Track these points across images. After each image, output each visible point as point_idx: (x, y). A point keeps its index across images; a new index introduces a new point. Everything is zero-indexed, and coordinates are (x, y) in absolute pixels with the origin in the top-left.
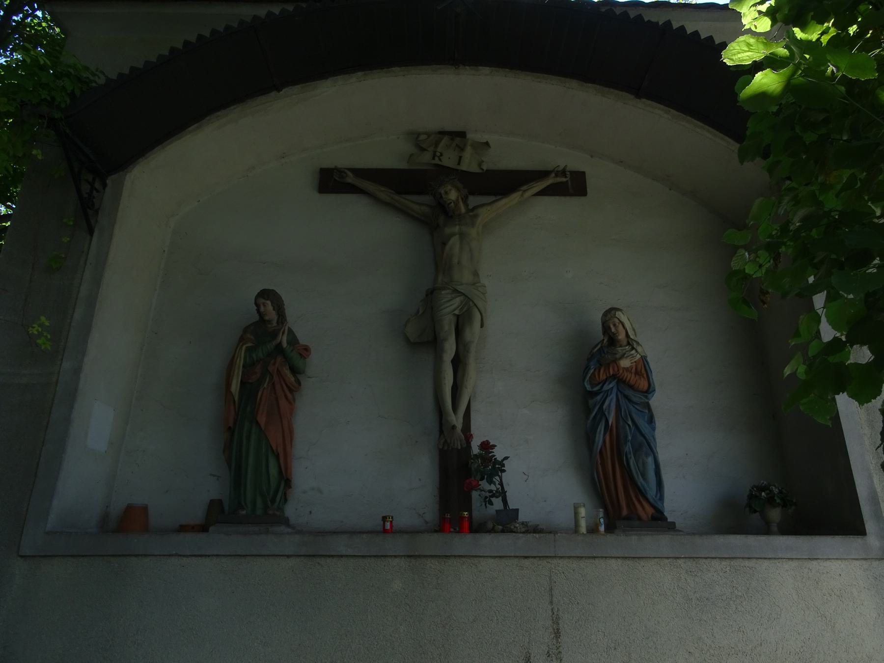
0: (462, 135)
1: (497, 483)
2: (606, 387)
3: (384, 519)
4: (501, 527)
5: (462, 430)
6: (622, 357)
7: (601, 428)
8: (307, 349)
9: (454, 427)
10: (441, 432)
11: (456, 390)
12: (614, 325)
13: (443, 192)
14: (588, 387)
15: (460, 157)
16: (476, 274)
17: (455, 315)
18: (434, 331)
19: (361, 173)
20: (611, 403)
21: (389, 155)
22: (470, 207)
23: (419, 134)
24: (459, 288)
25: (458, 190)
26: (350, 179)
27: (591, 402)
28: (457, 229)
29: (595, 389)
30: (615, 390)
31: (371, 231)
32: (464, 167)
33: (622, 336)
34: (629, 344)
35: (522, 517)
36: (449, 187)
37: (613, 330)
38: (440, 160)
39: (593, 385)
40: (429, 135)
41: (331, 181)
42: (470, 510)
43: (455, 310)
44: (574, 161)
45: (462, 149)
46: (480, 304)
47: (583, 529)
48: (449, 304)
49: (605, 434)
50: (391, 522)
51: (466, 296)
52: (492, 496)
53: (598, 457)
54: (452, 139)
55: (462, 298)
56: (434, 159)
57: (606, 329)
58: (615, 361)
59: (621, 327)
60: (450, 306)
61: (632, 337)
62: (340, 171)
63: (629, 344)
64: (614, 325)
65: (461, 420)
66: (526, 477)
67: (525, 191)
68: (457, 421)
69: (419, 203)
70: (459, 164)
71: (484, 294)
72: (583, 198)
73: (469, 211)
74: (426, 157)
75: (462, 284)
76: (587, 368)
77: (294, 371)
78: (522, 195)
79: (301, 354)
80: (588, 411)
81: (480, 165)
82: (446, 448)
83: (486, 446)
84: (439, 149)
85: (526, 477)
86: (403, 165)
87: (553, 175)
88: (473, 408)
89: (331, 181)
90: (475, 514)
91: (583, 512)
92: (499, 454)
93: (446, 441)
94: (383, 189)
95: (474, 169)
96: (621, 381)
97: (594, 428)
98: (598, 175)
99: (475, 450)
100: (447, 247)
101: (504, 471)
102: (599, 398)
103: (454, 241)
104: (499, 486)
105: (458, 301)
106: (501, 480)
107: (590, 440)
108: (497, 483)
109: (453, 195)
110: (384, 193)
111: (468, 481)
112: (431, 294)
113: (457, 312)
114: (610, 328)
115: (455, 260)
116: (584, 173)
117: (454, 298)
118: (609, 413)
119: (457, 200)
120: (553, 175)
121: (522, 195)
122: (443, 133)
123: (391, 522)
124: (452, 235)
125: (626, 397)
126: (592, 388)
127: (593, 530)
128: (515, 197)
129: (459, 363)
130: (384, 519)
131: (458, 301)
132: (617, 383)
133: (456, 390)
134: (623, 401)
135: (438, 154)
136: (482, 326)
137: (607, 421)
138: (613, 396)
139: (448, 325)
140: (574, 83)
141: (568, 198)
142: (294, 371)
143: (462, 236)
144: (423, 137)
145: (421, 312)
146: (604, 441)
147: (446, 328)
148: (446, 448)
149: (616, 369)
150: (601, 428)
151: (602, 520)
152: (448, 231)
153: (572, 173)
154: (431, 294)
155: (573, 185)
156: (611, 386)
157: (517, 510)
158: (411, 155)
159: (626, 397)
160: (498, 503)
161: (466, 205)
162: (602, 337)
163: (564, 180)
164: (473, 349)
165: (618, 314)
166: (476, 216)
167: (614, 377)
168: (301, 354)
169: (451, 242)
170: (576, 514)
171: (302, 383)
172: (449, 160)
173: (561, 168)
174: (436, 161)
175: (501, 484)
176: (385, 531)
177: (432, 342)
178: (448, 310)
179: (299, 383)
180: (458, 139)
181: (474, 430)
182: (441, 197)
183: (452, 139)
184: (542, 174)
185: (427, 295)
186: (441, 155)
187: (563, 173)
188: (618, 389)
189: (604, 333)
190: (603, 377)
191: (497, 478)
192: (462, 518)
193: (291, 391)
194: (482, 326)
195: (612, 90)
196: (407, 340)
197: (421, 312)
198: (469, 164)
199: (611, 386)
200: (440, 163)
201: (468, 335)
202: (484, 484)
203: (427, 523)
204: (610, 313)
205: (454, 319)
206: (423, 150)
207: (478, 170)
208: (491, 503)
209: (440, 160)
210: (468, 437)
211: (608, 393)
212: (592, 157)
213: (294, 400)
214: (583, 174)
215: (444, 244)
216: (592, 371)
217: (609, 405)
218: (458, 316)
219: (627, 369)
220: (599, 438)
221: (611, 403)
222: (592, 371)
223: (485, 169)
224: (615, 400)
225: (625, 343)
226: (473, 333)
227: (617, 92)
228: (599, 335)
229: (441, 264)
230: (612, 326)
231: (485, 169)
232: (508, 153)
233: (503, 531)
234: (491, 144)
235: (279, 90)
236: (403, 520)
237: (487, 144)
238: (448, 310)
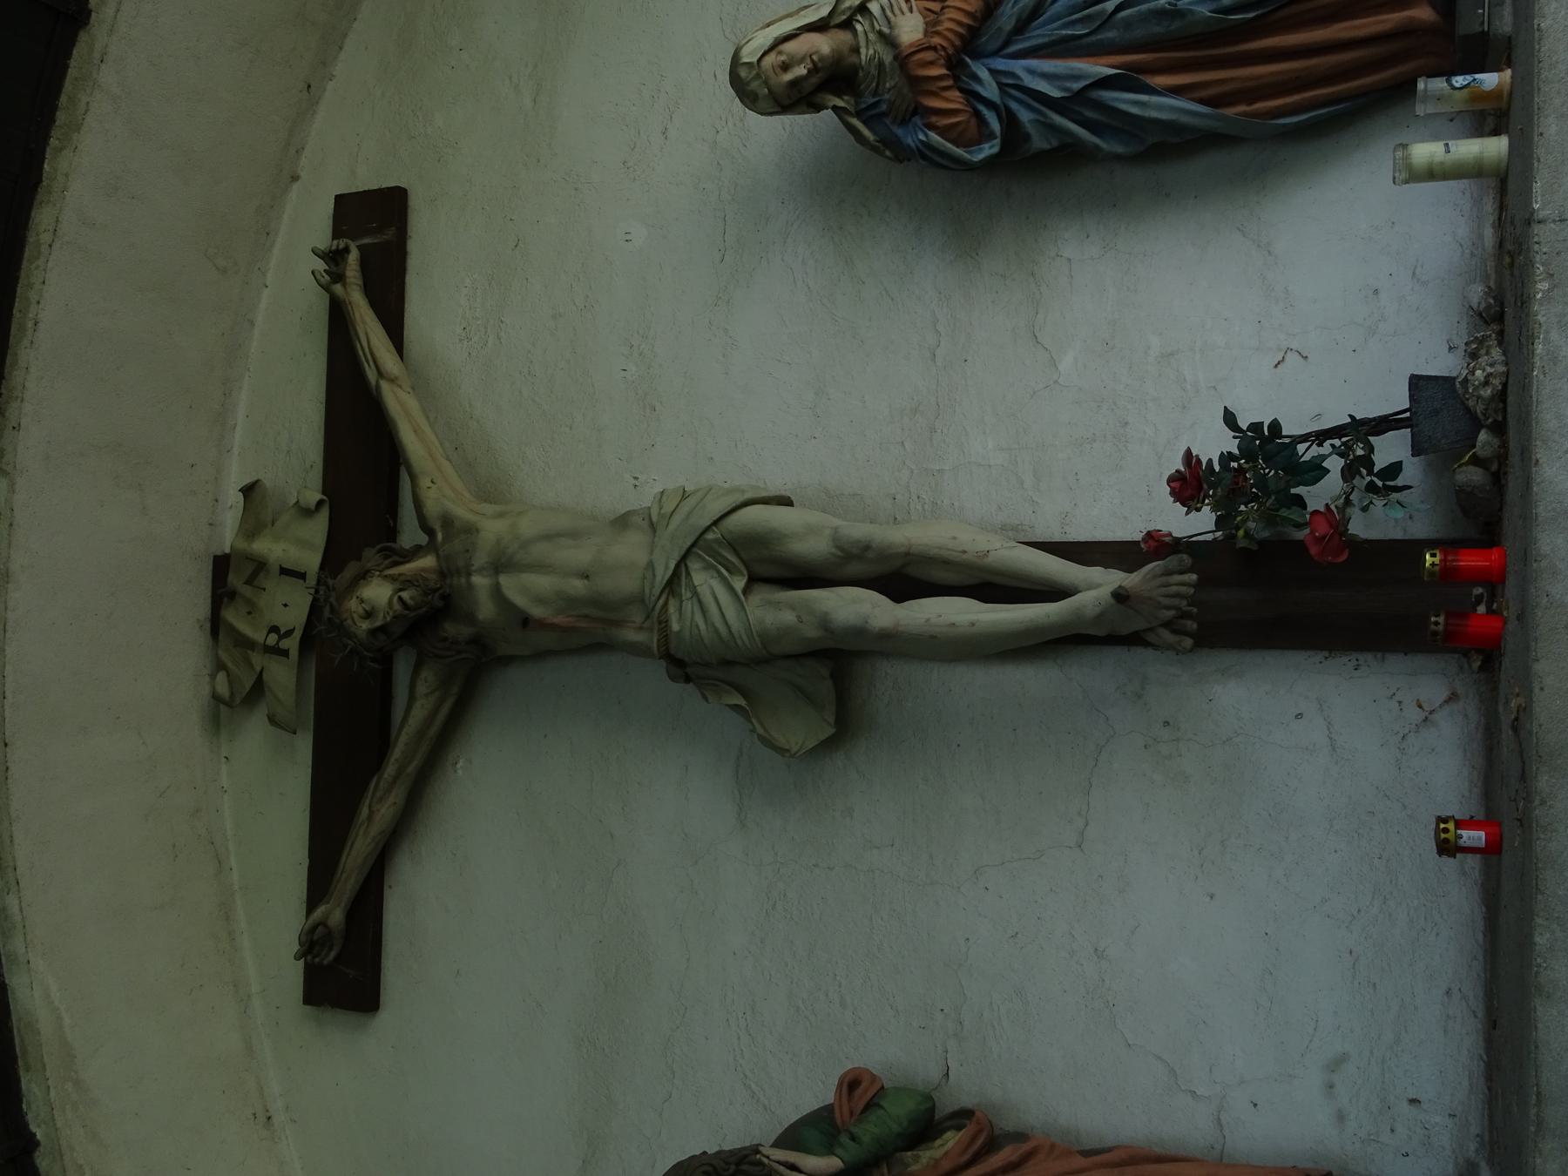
0: (221, 565)
1: (1315, 450)
2: (990, 90)
3: (1447, 848)
4: (1483, 436)
5: (1130, 571)
6: (889, 40)
7: (1124, 101)
8: (852, 1083)
9: (1120, 596)
10: (1135, 640)
11: (993, 586)
12: (785, 67)
13: (365, 625)
14: (988, 150)
15: (285, 572)
16: (622, 522)
17: (746, 591)
18: (804, 657)
19: (319, 885)
20: (1044, 75)
21: (266, 791)
22: (423, 539)
23: (216, 697)
24: (663, 574)
25: (364, 576)
26: (334, 913)
27: (1039, 142)
28: (480, 581)
29: (995, 125)
30: (1000, 64)
31: (524, 843)
32: (311, 561)
33: (823, 44)
34: (847, 25)
35: (1442, 363)
36: (353, 604)
37: (801, 71)
38: (289, 633)
39: (984, 135)
40: (220, 666)
41: (344, 972)
42: (1414, 548)
43: (731, 589)
44: (308, 223)
45: (260, 566)
46: (716, 507)
47: (1495, 147)
48: (713, 609)
49: (1152, 91)
50: (1459, 824)
51: (683, 559)
52: (1367, 461)
53: (1230, 111)
54: (232, 595)
55: (694, 565)
56: (285, 653)
57: (795, 98)
58: (903, 60)
59: (789, 47)
60: (720, 605)
61: (825, 12)
62: (311, 944)
63: (847, 25)
64: (785, 67)
65: (1095, 573)
66: (1292, 358)
67: (380, 374)
68: (1097, 586)
69: (415, 701)
70: (302, 576)
71: (685, 495)
72: (416, 202)
73: (432, 547)
74: (281, 676)
75: (650, 565)
76: (928, 155)
77: (925, 1128)
78: (393, 380)
79: (869, 1106)
80: (1069, 156)
81: (307, 512)
82: (1192, 625)
83: (1190, 484)
84: (259, 636)
85: (1292, 358)
86: (304, 746)
87: (338, 288)
88: (1057, 537)
89: (344, 972)
90: (1420, 529)
91: (1426, 151)
92: (1214, 444)
93: (1167, 625)
94: (365, 812)
95: (317, 530)
96: (970, 44)
97: (1130, 126)
98: (345, 159)
99: (1200, 523)
100: (537, 612)
101: (1275, 426)
102: (1025, 116)
103: (521, 589)
104: (1326, 448)
105: (702, 579)
106: (1304, 438)
107: (1164, 148)
108: (1315, 450)
109: (378, 592)
110: (378, 812)
111: (1313, 550)
112: (688, 666)
113: (739, 583)
114: (794, 83)
115: (577, 586)
116: (339, 199)
117: (695, 594)
118: (1076, 77)
119: (393, 579)
120: (338, 288)
121: (393, 380)
122: (216, 625)
123: (1459, 824)
124: (497, 592)
125: (1022, 27)
126: (992, 136)
127: (1489, 116)
128: (399, 402)
129: (904, 578)
130: (1447, 848)
131: (702, 579)
132: (977, 56)
133: (993, 586)
134: (1039, 35)
135: (272, 639)
136: (786, 502)
137: (1105, 83)
138: (1018, 66)
139: (779, 612)
140: (42, 217)
141: (413, 246)
142: (925, 1128)
143: (501, 564)
144: (223, 688)
145: (742, 702)
146: (1176, 91)
147: (788, 617)
148: (1192, 625)
149: (929, 56)
150: (1124, 101)
151: (1459, 81)
152: (486, 610)
153: (337, 233)
154: (688, 666)
155: (374, 231)
156: (984, 74)
157: (1416, 382)
158: (272, 720)
159: (1022, 27)
160: (1390, 448)
161: (417, 551)
162: (827, 114)
163: (353, 256)
164: (858, 531)
165: (749, 55)
166: (447, 521)
167: (956, 66)
168: (869, 1106)
169: (519, 600)
170: (1432, 174)
171: (966, 1101)
172: (288, 607)
173: (321, 265)
174: (292, 644)
175: (1321, 436)
176: (1492, 849)
177: (836, 675)
178: (731, 613)
179: (963, 1116)
180: (235, 580)
181: (1130, 530)
182: (382, 629)
183: (232, 595)
184: (339, 321)
185: (688, 679)
186: (274, 629)
187: (334, 258)
188: (996, 53)
189: (817, 108)
190: (953, 100)
191: (1301, 448)
192: (1447, 573)
193: (993, 1143)
194: (786, 502)
195: (63, 99)
196: (829, 745)
197: (742, 702)
198: (300, 544)
199: (984, 74)
200: (298, 634)
201: (814, 547)
202: (1320, 495)
203: (1453, 697)
204: (755, 89)
205: (763, 594)
206: (258, 689)
207: (323, 518)
208: (1394, 469)
209: (289, 633)
210: (1157, 546)
211: (1010, 85)
212: (295, 178)
213: (1020, 1137)
214: (342, 202)
215: (526, 621)
216: (935, 138)
217: (1045, 76)
218: (754, 580)
219: (931, 27)
220: (1157, 105)
221: (1044, 75)
222: (935, 138)
223: (318, 496)
224: (1034, 63)
225: (844, 37)
226: (806, 531)
227: (68, 85)
228: (813, 128)
229: (587, 633)
230: (788, 77)
231: (318, 496)
232: (278, 430)
233: (1499, 429)
234: (248, 480)
235: (31, 1143)
236: (1443, 774)
237: (248, 491)
238: (731, 613)
